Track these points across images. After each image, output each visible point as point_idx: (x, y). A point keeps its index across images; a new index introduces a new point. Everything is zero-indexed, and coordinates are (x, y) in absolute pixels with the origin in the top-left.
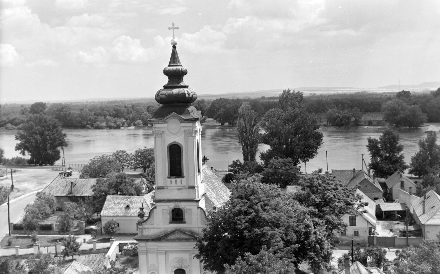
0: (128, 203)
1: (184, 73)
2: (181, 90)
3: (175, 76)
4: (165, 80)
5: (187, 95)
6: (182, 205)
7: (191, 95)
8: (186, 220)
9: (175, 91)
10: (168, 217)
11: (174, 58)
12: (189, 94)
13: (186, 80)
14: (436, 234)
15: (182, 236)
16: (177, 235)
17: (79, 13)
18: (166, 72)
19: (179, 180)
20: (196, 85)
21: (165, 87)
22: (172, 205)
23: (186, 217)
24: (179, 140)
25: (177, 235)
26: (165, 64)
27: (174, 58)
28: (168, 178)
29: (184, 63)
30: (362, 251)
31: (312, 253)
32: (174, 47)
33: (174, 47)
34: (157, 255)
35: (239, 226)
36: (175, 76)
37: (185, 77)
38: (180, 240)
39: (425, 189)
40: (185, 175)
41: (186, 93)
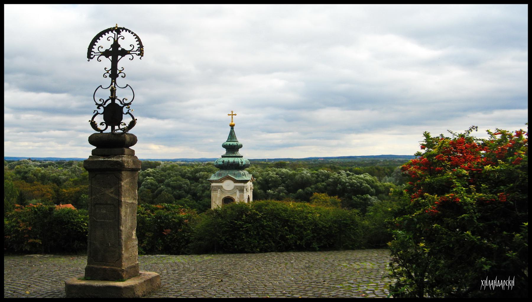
2: (236, 160)
3: (232, 149)
4: (224, 151)
5: (240, 163)
7: (244, 163)
9: (231, 160)
11: (232, 136)
12: (242, 162)
13: (240, 152)
18: (224, 146)
26: (224, 139)
27: (232, 136)
29: (240, 140)
30: (418, 226)
31: (182, 215)
32: (232, 126)
33: (232, 126)
34: (112, 143)
35: (64, 190)
36: (232, 149)
37: (240, 150)
41: (240, 161)
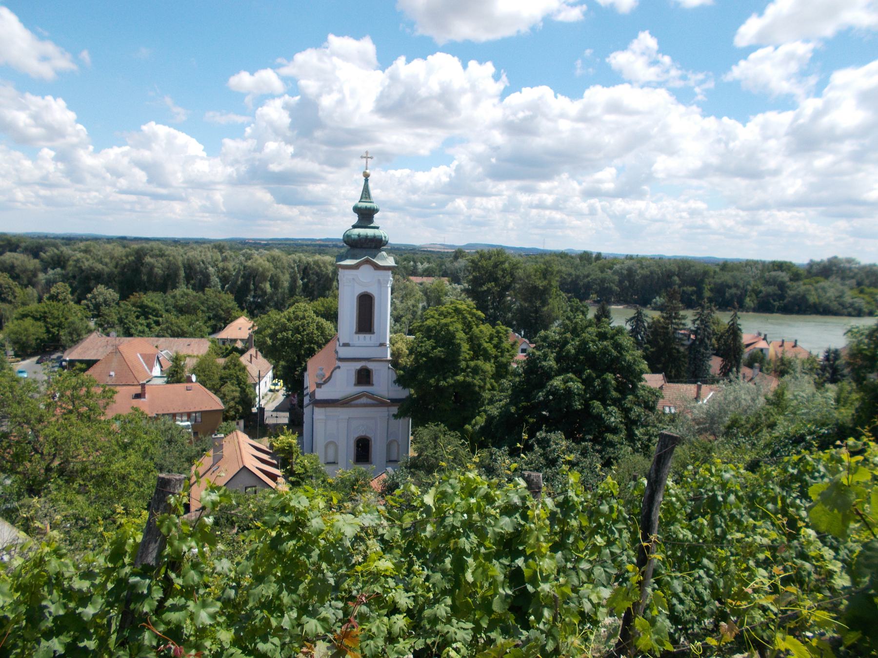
0: (136, 403)
1: (375, 211)
3: (366, 215)
4: (354, 219)
6: (370, 365)
8: (374, 382)
10: (353, 378)
11: (366, 193)
14: (396, 416)
15: (370, 401)
16: (364, 400)
17: (219, 183)
18: (356, 209)
19: (368, 336)
20: (389, 227)
21: (354, 227)
22: (358, 365)
23: (375, 378)
24: (372, 290)
25: (364, 400)
27: (366, 193)
28: (356, 333)
36: (366, 215)
37: (376, 216)
38: (365, 405)
39: (40, 426)
40: (375, 331)
